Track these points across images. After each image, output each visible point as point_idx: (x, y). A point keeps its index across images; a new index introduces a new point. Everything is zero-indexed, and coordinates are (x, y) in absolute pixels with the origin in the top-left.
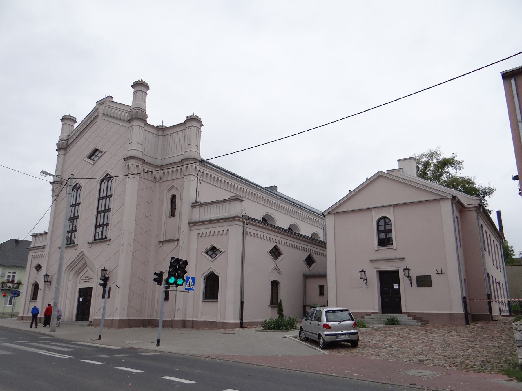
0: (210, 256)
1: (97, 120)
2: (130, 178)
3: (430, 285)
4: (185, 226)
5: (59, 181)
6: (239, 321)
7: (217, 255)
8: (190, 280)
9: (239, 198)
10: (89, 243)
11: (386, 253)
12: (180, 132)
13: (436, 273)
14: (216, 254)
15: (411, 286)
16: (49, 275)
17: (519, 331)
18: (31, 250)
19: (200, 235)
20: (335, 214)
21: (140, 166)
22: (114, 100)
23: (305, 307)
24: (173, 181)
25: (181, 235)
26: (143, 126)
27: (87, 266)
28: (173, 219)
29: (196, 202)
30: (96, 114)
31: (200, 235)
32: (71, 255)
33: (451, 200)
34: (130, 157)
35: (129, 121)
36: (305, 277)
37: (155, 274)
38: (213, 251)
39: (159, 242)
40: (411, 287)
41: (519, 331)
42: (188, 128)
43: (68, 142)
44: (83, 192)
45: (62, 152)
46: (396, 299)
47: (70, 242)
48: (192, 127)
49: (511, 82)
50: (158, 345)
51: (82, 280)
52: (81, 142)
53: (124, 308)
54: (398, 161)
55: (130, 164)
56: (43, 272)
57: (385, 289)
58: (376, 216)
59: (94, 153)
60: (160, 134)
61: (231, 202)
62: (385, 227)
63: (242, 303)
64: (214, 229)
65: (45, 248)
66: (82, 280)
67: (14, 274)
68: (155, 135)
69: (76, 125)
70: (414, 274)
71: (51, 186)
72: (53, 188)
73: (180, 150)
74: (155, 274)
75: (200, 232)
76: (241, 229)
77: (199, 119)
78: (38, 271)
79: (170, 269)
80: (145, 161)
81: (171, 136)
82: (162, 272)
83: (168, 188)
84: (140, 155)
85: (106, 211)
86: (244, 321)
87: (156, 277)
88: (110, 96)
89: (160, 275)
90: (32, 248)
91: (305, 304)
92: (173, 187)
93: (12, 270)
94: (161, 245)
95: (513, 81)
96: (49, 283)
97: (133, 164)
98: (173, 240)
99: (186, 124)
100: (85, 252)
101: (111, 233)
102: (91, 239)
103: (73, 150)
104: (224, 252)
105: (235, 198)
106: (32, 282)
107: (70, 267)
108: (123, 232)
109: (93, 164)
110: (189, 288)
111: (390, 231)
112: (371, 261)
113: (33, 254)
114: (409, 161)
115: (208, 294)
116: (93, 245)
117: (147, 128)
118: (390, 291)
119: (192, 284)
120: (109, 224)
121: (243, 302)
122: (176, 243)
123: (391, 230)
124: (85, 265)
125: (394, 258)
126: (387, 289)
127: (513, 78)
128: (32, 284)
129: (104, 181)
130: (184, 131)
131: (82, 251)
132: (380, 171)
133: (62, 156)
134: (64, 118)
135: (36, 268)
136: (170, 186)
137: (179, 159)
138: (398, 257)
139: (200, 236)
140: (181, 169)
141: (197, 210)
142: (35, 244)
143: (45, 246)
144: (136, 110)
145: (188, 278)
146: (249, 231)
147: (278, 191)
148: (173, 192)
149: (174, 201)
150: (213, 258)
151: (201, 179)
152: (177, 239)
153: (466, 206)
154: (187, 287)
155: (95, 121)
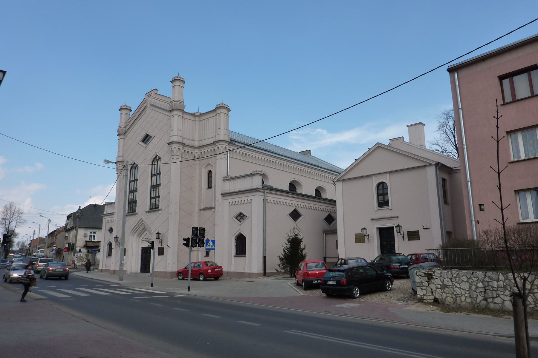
0: (239, 220)
1: (146, 110)
2: (174, 159)
3: (418, 238)
4: (219, 197)
5: (121, 161)
6: (263, 272)
7: (244, 219)
8: (211, 243)
9: (259, 173)
10: (147, 212)
11: (384, 212)
12: (210, 118)
13: (423, 229)
14: (243, 219)
15: (404, 239)
16: (118, 237)
17: (418, 276)
18: (104, 216)
19: (231, 203)
20: (343, 181)
21: (181, 148)
22: (158, 92)
23: (325, 258)
24: (209, 159)
25: (216, 205)
26: (181, 115)
27: (146, 230)
28: (210, 190)
29: (227, 176)
30: (145, 105)
31: (231, 203)
32: (132, 221)
33: (435, 166)
34: (172, 142)
35: (170, 111)
36: (325, 233)
37: (184, 240)
38: (241, 217)
39: (200, 209)
40: (404, 240)
41: (418, 276)
42: (218, 115)
43: (126, 128)
44: (140, 169)
45: (122, 137)
46: (385, 251)
47: (132, 211)
48: (221, 114)
49: (454, 75)
50: (189, 290)
51: (143, 240)
52: (136, 128)
53: (174, 263)
54: (408, 126)
55: (173, 147)
56: (114, 234)
57: (384, 243)
58: (375, 181)
59: (146, 139)
60: (196, 120)
61: (253, 176)
62: (383, 191)
63: (264, 257)
64: (241, 199)
65: (114, 215)
66: (143, 240)
67: (94, 234)
68: (193, 121)
69: (131, 113)
70: (405, 229)
71: (115, 165)
72: (117, 167)
73: (209, 135)
74: (184, 240)
75: (231, 201)
76: (262, 198)
77: (227, 107)
78: (111, 233)
79: (192, 236)
80: (184, 144)
81: (209, 120)
82: (188, 238)
83: (205, 165)
84: (181, 140)
85: (157, 186)
86: (267, 271)
87: (185, 242)
88: (155, 89)
89: (187, 240)
90: (105, 214)
91: (325, 256)
92: (209, 164)
93: (93, 231)
94: (202, 211)
95: (456, 75)
96: (119, 244)
97: (175, 148)
98: (211, 208)
99: (216, 111)
100: (144, 219)
101: (162, 204)
102: (148, 209)
103: (130, 134)
104: (249, 217)
105: (255, 173)
106: (107, 242)
107: (133, 230)
108: (170, 203)
109: (146, 147)
110: (210, 248)
111: (387, 194)
112: (372, 220)
113: (107, 219)
114: (417, 126)
115: (238, 251)
116: (150, 213)
117: (186, 116)
118: (388, 244)
119: (212, 245)
120: (160, 196)
121: (265, 256)
122: (213, 210)
123: (388, 193)
124: (145, 229)
125: (390, 217)
126: (385, 243)
127: (456, 72)
128: (107, 243)
129: (155, 161)
130: (215, 117)
131: (142, 218)
132: (378, 143)
133: (122, 140)
134: (121, 108)
135: (109, 231)
136: (206, 164)
137: (211, 141)
138: (394, 216)
139: (231, 204)
140: (214, 149)
141: (227, 183)
142: (107, 211)
143: (114, 213)
144: (175, 102)
145: (208, 241)
146: (269, 199)
147: (312, 155)
148: (209, 168)
149: (210, 176)
150: (241, 222)
151: (231, 156)
152: (213, 207)
153: (454, 169)
154: (207, 248)
155: (145, 111)
